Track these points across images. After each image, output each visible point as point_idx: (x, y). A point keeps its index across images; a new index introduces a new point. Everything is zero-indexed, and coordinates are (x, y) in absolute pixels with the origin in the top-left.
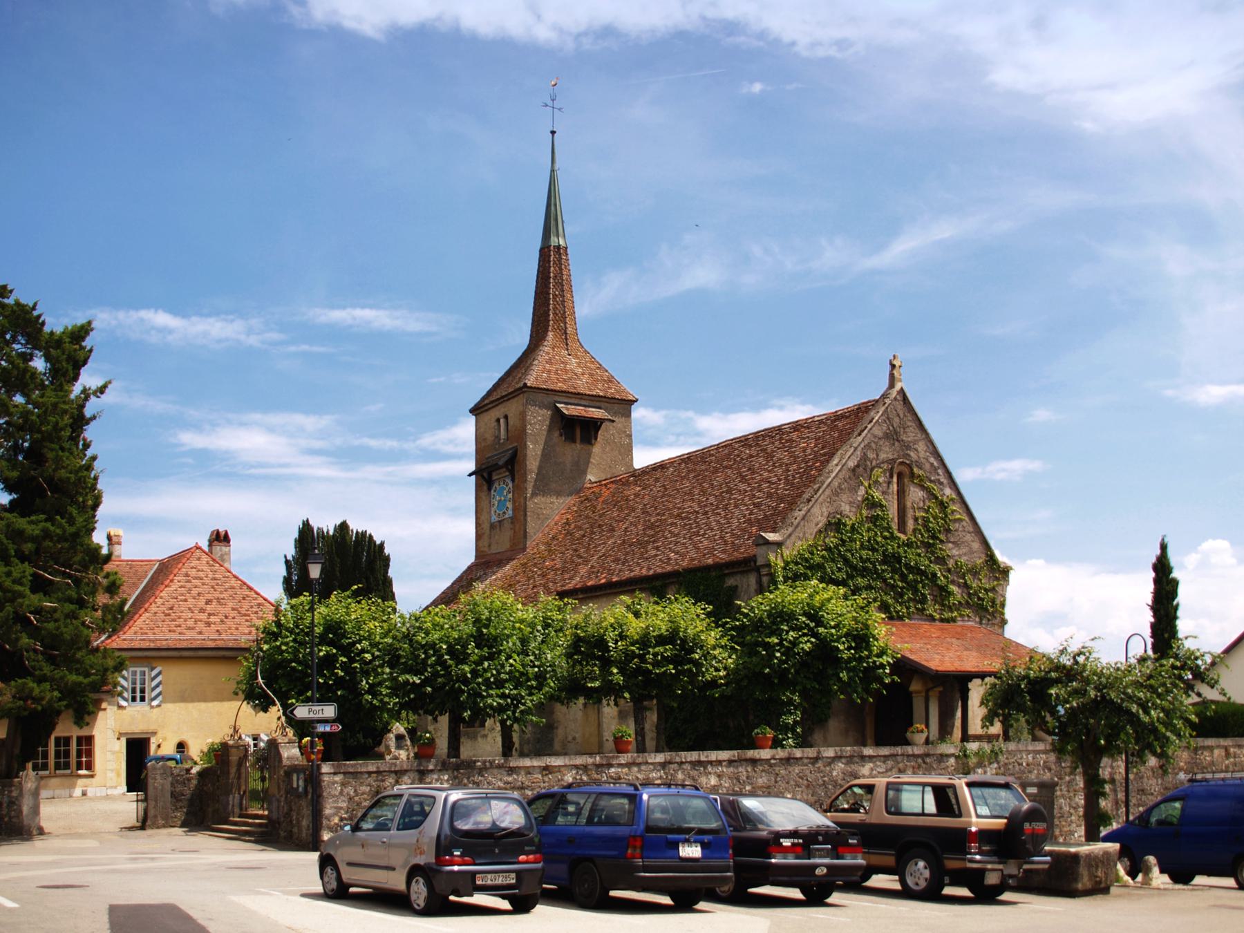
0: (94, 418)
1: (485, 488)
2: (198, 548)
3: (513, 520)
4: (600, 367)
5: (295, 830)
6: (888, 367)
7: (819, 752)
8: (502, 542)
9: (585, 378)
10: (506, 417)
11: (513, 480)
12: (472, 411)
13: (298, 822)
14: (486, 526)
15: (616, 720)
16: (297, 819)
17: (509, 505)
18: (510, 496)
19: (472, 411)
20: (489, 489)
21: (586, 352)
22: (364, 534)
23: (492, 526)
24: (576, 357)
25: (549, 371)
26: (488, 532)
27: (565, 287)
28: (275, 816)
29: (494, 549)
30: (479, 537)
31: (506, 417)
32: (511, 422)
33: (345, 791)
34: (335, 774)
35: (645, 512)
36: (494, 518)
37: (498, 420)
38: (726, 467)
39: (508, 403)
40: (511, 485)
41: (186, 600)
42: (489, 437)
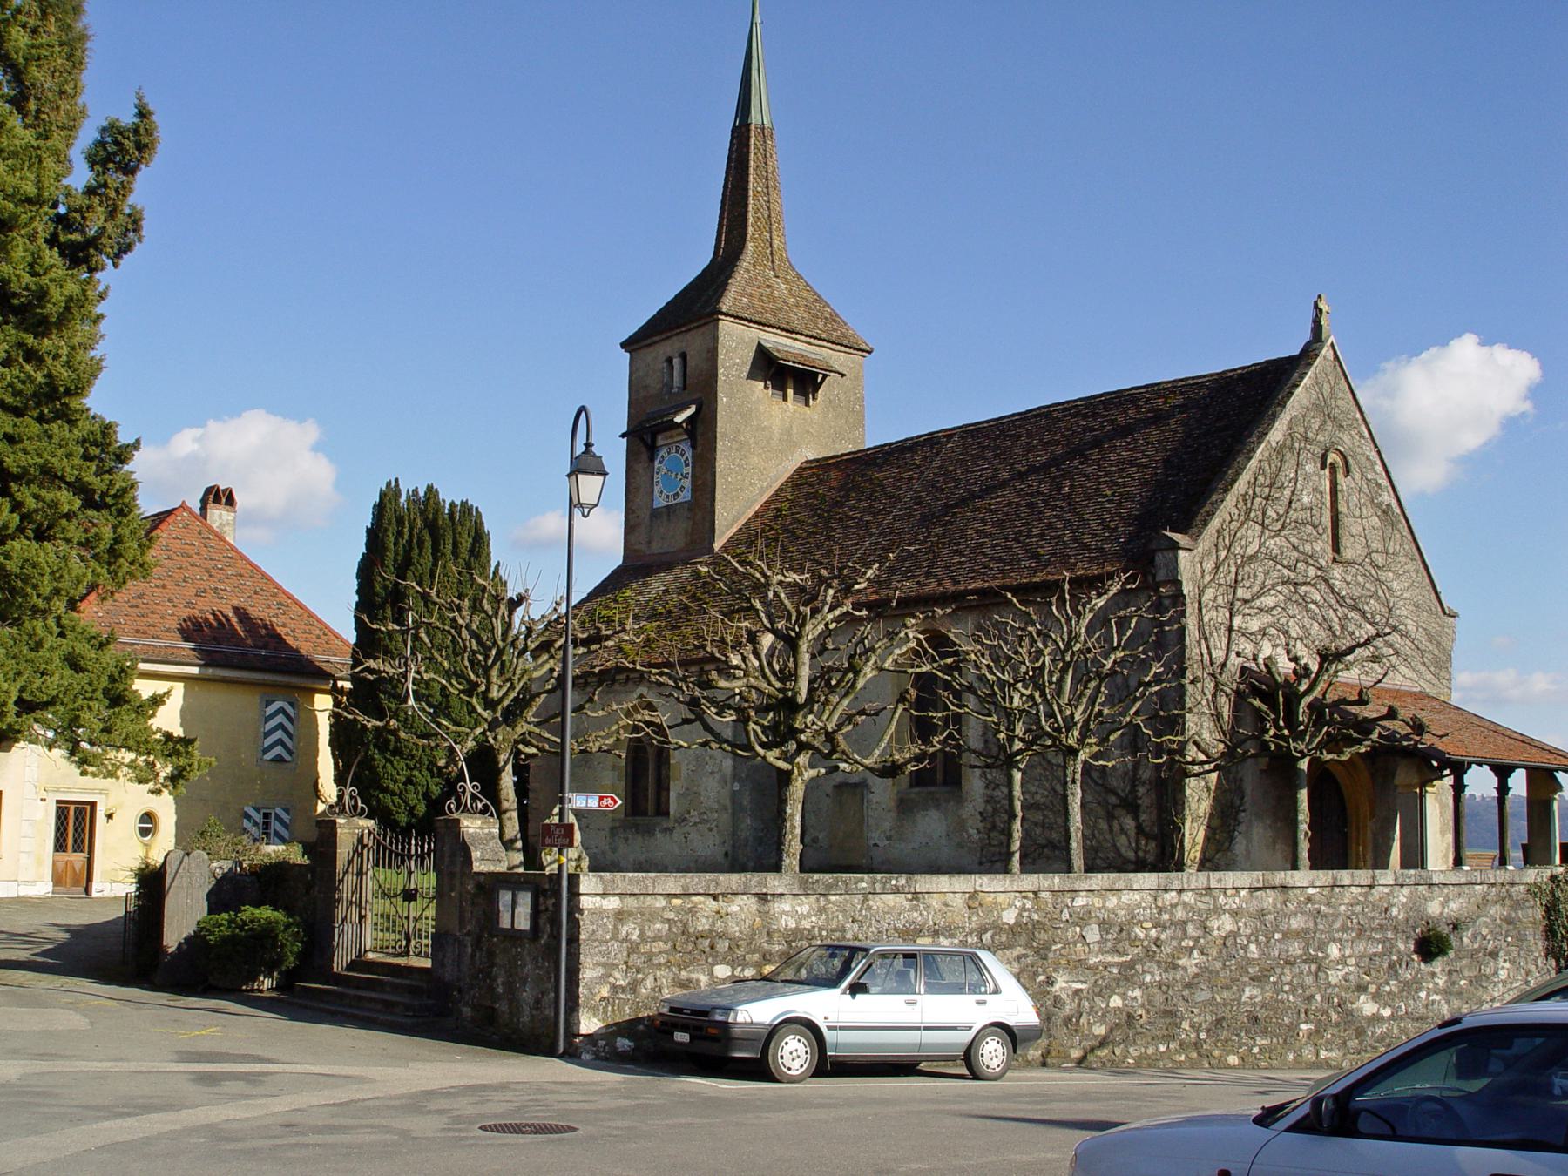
0: (143, 113)
1: (645, 456)
2: (183, 506)
3: (692, 506)
4: (819, 299)
5: (502, 1006)
6: (1311, 313)
7: (1373, 877)
8: (673, 537)
9: (800, 312)
10: (684, 356)
11: (694, 447)
12: (623, 345)
13: (510, 988)
14: (644, 513)
15: (893, 814)
16: (510, 986)
17: (687, 483)
18: (688, 470)
19: (623, 345)
20: (652, 460)
21: (799, 277)
22: (466, 509)
23: (656, 514)
24: (786, 281)
25: (751, 295)
26: (647, 520)
27: (771, 183)
28: (448, 974)
29: (656, 548)
30: (630, 529)
31: (684, 356)
32: (691, 363)
33: (624, 930)
34: (604, 895)
35: (918, 501)
36: (660, 502)
37: (670, 361)
38: (1049, 443)
39: (688, 336)
40: (689, 454)
41: (164, 586)
42: (654, 384)
